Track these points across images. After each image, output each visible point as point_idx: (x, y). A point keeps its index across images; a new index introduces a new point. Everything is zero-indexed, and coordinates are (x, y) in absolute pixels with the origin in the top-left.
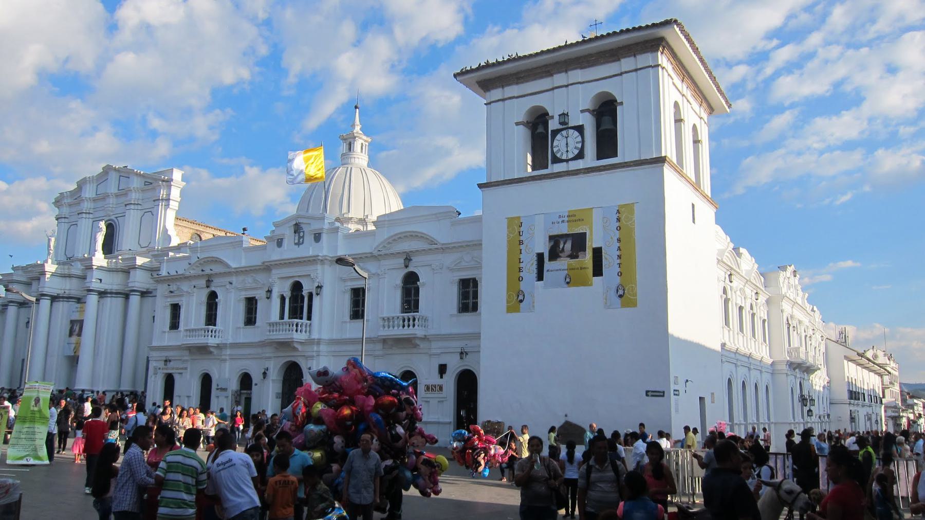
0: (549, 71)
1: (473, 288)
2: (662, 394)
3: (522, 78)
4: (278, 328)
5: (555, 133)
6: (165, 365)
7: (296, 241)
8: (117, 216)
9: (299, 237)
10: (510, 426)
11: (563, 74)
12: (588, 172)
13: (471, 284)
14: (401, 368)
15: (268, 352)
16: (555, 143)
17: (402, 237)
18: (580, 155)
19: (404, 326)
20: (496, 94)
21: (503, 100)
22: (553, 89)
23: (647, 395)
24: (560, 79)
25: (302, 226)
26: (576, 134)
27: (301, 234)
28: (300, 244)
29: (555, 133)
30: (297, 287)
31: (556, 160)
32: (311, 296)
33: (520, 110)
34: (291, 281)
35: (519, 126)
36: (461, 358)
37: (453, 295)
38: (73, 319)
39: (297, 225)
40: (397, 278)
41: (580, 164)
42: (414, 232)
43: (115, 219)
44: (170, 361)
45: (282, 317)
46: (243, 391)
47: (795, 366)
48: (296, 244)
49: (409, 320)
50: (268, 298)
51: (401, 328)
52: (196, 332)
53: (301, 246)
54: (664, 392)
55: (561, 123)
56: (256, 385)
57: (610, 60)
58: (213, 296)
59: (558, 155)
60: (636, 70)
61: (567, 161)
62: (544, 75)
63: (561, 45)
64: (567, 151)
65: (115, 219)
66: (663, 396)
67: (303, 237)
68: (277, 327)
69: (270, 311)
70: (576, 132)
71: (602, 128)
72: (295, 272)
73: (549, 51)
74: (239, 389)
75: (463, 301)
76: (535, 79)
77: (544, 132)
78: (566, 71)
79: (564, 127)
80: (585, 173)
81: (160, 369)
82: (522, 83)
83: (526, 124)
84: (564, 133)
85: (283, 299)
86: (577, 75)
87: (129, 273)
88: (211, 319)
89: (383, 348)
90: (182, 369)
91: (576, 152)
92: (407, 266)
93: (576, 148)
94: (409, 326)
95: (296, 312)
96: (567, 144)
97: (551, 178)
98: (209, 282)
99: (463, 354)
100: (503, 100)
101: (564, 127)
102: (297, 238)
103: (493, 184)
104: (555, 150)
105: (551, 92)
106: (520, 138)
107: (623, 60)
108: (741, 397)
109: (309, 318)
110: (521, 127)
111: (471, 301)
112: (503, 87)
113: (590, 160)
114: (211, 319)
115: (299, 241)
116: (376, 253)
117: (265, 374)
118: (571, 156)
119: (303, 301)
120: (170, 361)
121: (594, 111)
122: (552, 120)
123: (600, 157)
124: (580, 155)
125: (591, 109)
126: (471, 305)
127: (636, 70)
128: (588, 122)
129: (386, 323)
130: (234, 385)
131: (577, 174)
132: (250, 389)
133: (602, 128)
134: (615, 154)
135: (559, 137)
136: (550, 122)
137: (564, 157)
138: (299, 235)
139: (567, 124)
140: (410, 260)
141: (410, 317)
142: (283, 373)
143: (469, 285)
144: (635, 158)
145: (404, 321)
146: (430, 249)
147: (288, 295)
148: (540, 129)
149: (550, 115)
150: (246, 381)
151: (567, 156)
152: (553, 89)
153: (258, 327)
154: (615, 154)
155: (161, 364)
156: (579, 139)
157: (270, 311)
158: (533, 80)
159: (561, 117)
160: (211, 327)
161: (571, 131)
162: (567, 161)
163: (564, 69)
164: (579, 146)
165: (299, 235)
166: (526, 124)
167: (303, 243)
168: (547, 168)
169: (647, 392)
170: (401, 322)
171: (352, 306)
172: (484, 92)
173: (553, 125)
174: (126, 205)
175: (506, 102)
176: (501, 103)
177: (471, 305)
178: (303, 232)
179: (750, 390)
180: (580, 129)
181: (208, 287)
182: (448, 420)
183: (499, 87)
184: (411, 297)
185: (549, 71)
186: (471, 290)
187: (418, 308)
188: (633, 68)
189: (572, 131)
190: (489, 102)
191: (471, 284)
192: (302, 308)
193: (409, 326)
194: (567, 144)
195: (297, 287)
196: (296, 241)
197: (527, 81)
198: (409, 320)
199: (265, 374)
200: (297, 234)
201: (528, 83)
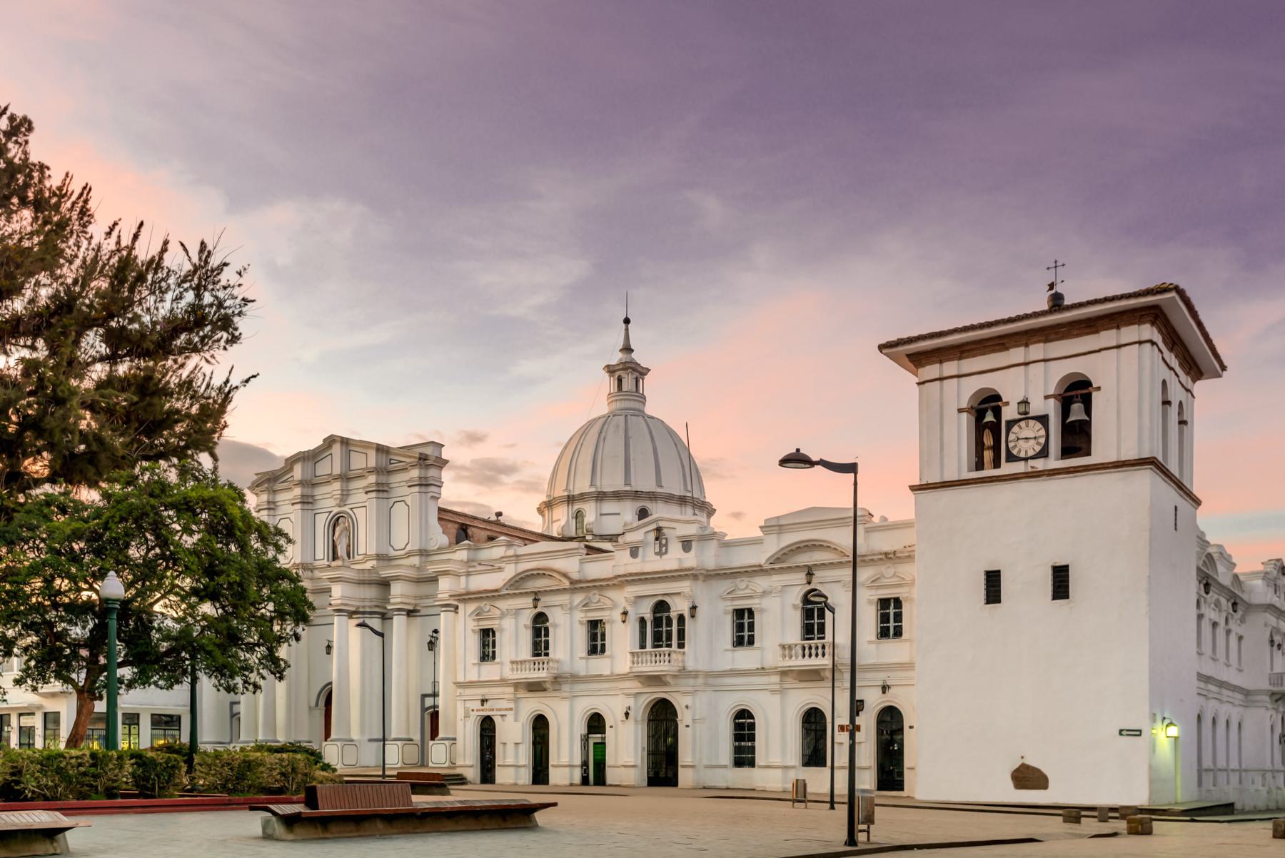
0: (1003, 344)
1: (895, 608)
2: (1138, 733)
3: (968, 351)
5: (1011, 424)
6: (482, 705)
7: (657, 550)
15: (634, 686)
16: (1012, 437)
18: (1044, 453)
19: (804, 656)
20: (932, 371)
21: (941, 379)
23: (1121, 734)
26: (1039, 426)
27: (664, 542)
29: (1011, 424)
30: (661, 607)
31: (1011, 458)
32: (681, 619)
37: (581, 637)
39: (659, 529)
41: (1040, 464)
44: (487, 700)
45: (643, 646)
46: (590, 736)
47: (1278, 697)
48: (656, 554)
53: (664, 557)
54: (1140, 731)
56: (611, 727)
57: (1086, 331)
58: (540, 618)
59: (1015, 452)
60: (1119, 347)
61: (1026, 459)
62: (997, 348)
66: (1140, 735)
67: (666, 545)
69: (621, 638)
71: (1071, 419)
74: (586, 732)
76: (984, 354)
77: (994, 420)
78: (960, 359)
79: (1023, 416)
80: (1049, 475)
81: (473, 710)
83: (968, 410)
84: (1023, 424)
85: (642, 621)
88: (540, 645)
89: (781, 681)
90: (506, 709)
92: (535, 607)
94: (817, 655)
99: (885, 689)
100: (941, 379)
101: (1023, 416)
102: (657, 546)
104: (1011, 445)
106: (960, 431)
108: (1210, 735)
109: (681, 646)
110: (965, 415)
112: (941, 362)
114: (540, 645)
116: (767, 567)
120: (487, 700)
123: (1067, 452)
127: (1119, 347)
128: (1051, 409)
129: (787, 652)
131: (1039, 476)
132: (603, 732)
133: (1071, 419)
134: (1088, 454)
135: (1015, 429)
140: (812, 574)
143: (889, 605)
144: (1113, 458)
145: (804, 648)
146: (841, 562)
147: (649, 617)
148: (989, 417)
150: (596, 723)
151: (1040, 437)
153: (758, 648)
154: (1088, 454)
155: (478, 705)
157: (621, 638)
158: (981, 355)
159: (1021, 405)
161: (1031, 422)
162: (1026, 459)
166: (968, 410)
167: (666, 552)
169: (1121, 731)
173: (1009, 413)
175: (945, 381)
176: (938, 382)
178: (666, 539)
179: (1234, 727)
180: (1043, 419)
181: (535, 607)
182: (631, 761)
185: (1174, 343)
186: (746, 621)
188: (1114, 344)
190: (922, 380)
195: (661, 607)
198: (817, 648)
199: (627, 714)
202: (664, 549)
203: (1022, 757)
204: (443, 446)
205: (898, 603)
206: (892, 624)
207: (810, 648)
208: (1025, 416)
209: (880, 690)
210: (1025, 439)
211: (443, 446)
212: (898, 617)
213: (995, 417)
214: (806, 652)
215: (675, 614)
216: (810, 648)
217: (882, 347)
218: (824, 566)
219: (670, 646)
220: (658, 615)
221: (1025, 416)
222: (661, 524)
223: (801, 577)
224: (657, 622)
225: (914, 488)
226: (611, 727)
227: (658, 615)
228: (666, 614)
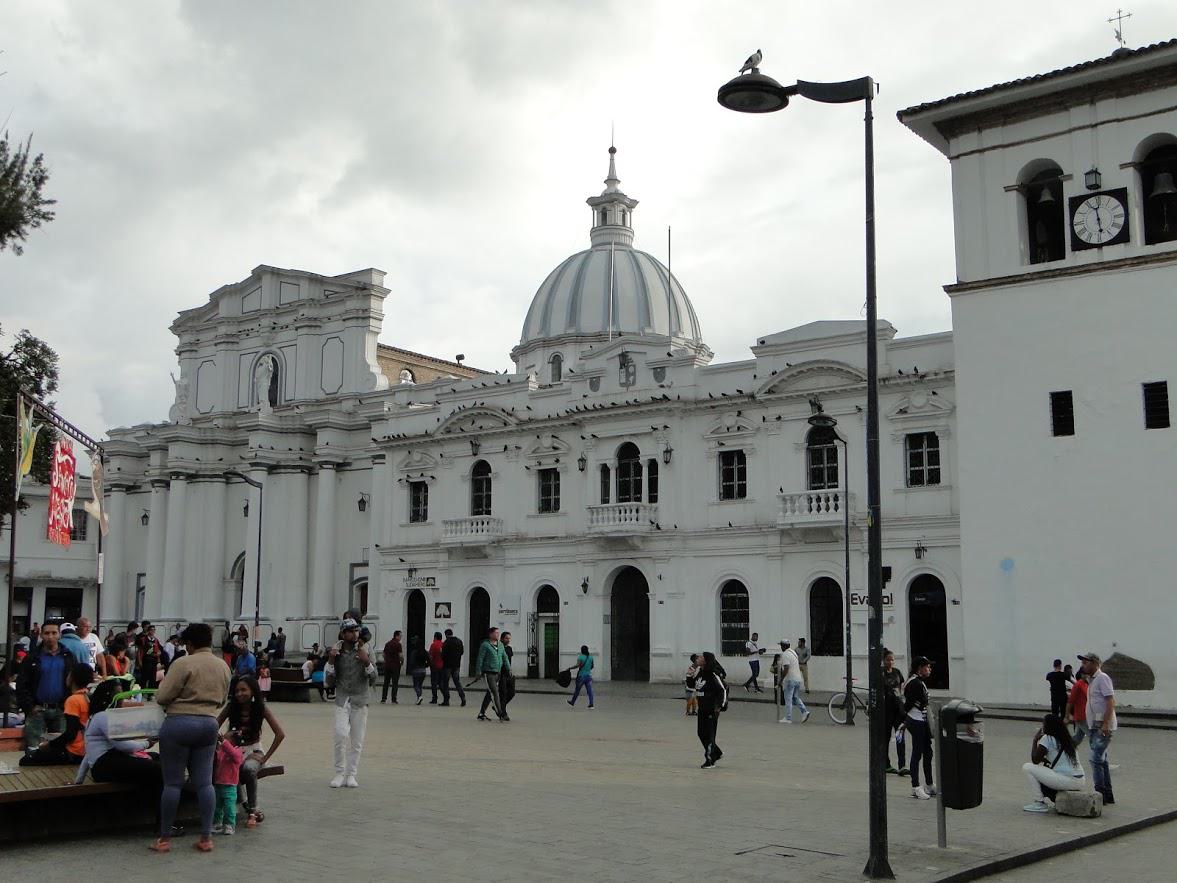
4: (606, 516)
5: (1076, 202)
7: (623, 380)
8: (279, 345)
9: (628, 375)
10: (1056, 661)
11: (1086, 107)
12: (1139, 264)
13: (736, 459)
14: (814, 574)
15: (588, 550)
16: (1077, 219)
17: (786, 378)
18: (1123, 237)
20: (968, 141)
22: (1070, 131)
24: (1080, 114)
25: (630, 356)
26: (1114, 202)
27: (631, 369)
28: (630, 385)
29: (1076, 202)
30: (628, 452)
31: (1079, 245)
33: (1012, 165)
34: (618, 444)
35: (1010, 193)
36: (919, 557)
37: (529, 490)
38: (492, 482)
40: (466, 466)
42: (824, 361)
43: (278, 351)
45: (605, 500)
46: (541, 614)
48: (622, 385)
49: (827, 500)
50: (582, 470)
51: (806, 512)
52: (457, 525)
53: (631, 388)
55: (1089, 187)
56: (566, 603)
59: (1083, 237)
61: (1099, 246)
63: (988, 87)
64: (1101, 231)
65: (278, 351)
67: (634, 374)
68: (598, 514)
69: (580, 490)
70: (1113, 199)
72: (624, 429)
73: (969, 96)
75: (913, 469)
78: (1092, 102)
79: (1092, 192)
80: (1133, 265)
82: (1014, 122)
84: (1092, 201)
85: (605, 470)
86: (1107, 108)
87: (316, 435)
88: (481, 503)
91: (1115, 231)
93: (1114, 225)
95: (628, 491)
96: (1099, 219)
97: (1071, 274)
98: (475, 446)
99: (920, 551)
100: (981, 151)
101: (1092, 192)
102: (623, 375)
103: (970, 285)
104: (1077, 229)
105: (1068, 135)
106: (1009, 217)
107: (1073, 110)
109: (653, 499)
111: (736, 483)
113: (1138, 246)
114: (481, 503)
115: (627, 380)
117: (585, 586)
118: (1106, 238)
119: (639, 472)
120: (415, 570)
121: (1140, 163)
122: (1070, 182)
124: (1123, 237)
125: (1137, 161)
126: (736, 489)
128: (1130, 181)
130: (529, 605)
132: (556, 609)
135: (1083, 208)
136: (1066, 185)
137: (1094, 240)
138: (627, 370)
139: (1099, 187)
141: (830, 495)
142: (613, 581)
147: (612, 463)
149: (1065, 173)
150: (548, 599)
152: (1070, 131)
156: (1121, 210)
157: (580, 490)
160: (654, 505)
161: (1105, 199)
162: (1099, 246)
163: (1089, 99)
164: (1121, 221)
165: (627, 370)
167: (634, 383)
168: (1063, 257)
170: (806, 504)
171: (722, 478)
172: (945, 138)
173: (1071, 190)
174: (296, 329)
177: (736, 489)
178: (634, 366)
180: (1121, 195)
183: (974, 130)
184: (822, 463)
185: (1060, 104)
186: (735, 467)
187: (836, 480)
189: (1107, 197)
191: (736, 459)
192: (639, 484)
193: (828, 509)
194: (1099, 219)
195: (628, 452)
196: (623, 380)
197: (1025, 119)
198: (827, 500)
199: (585, 586)
200: (624, 370)
201: (1052, 117)
202: (631, 378)
203: (1114, 645)
204: (385, 273)
205: (932, 439)
206: (926, 467)
207: (819, 499)
208: (1095, 189)
209: (406, 574)
210: (1094, 221)
211: (385, 273)
212: (934, 458)
213: (1052, 195)
214: (814, 504)
215: (646, 459)
216: (819, 499)
217: (901, 115)
218: (833, 394)
219: (639, 499)
220: (624, 461)
221: (1095, 189)
222: (628, 348)
223: (467, 448)
224: (623, 471)
225: (948, 289)
226: (566, 603)
227: (624, 461)
228: (634, 460)
